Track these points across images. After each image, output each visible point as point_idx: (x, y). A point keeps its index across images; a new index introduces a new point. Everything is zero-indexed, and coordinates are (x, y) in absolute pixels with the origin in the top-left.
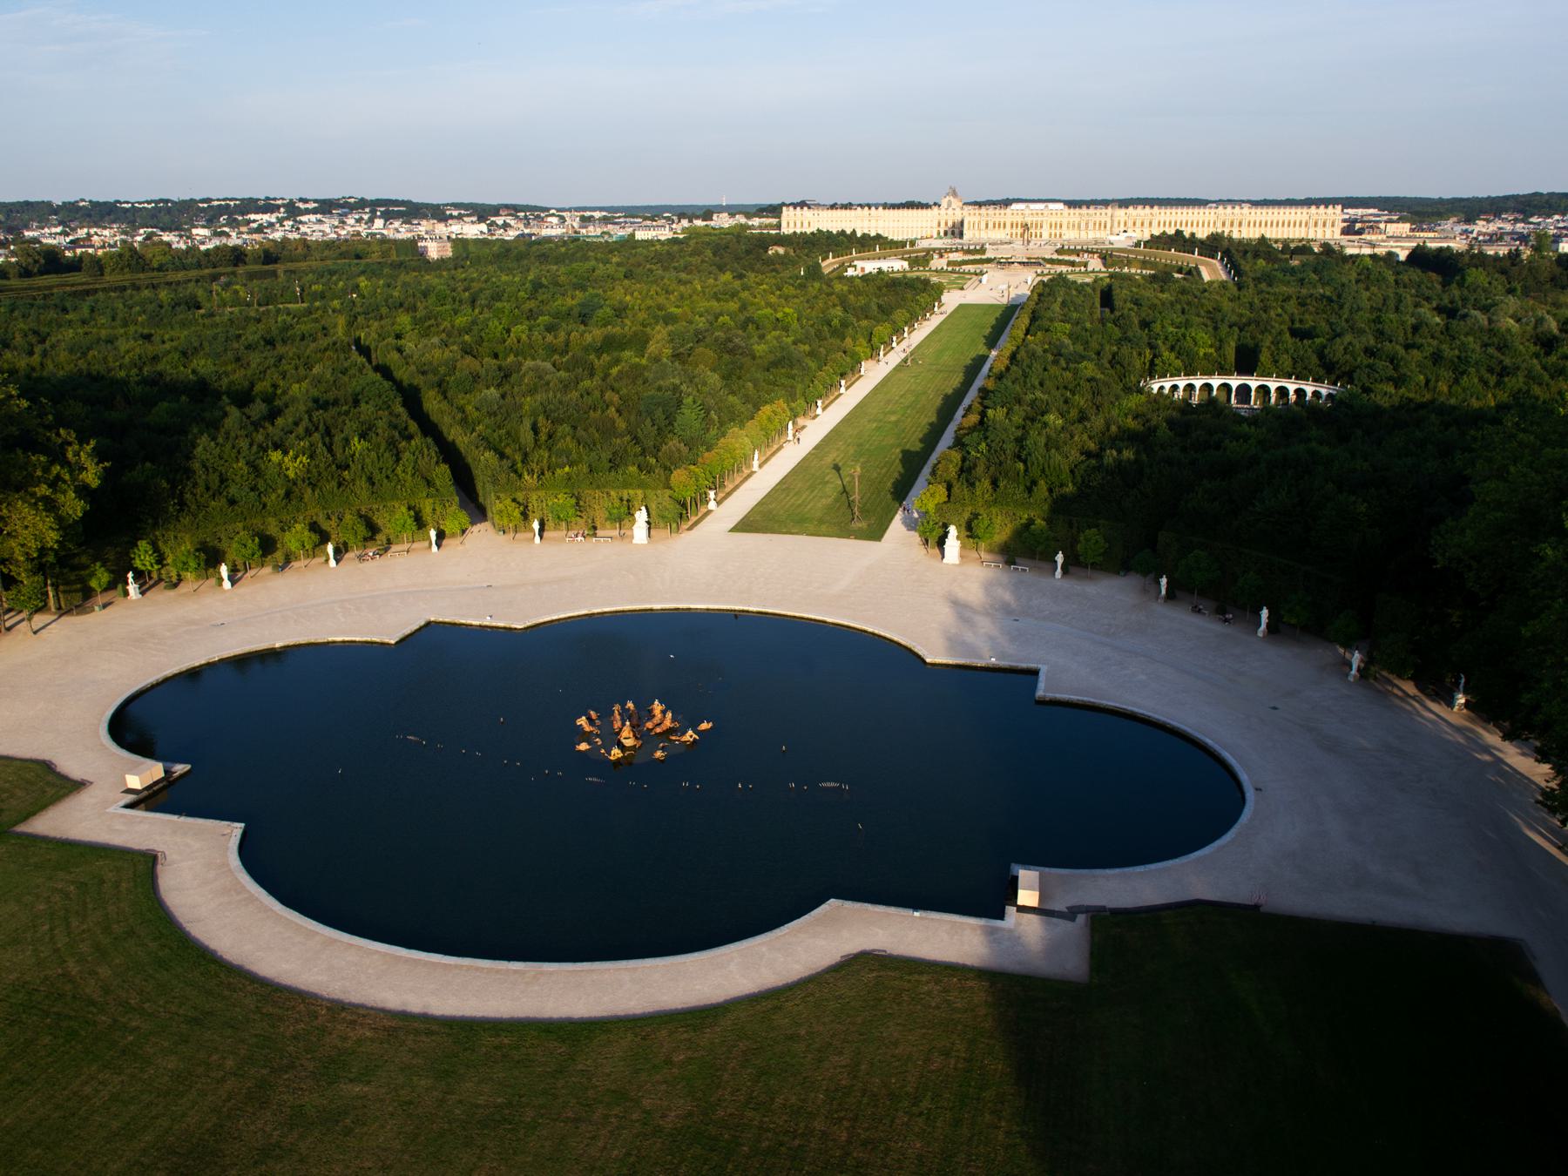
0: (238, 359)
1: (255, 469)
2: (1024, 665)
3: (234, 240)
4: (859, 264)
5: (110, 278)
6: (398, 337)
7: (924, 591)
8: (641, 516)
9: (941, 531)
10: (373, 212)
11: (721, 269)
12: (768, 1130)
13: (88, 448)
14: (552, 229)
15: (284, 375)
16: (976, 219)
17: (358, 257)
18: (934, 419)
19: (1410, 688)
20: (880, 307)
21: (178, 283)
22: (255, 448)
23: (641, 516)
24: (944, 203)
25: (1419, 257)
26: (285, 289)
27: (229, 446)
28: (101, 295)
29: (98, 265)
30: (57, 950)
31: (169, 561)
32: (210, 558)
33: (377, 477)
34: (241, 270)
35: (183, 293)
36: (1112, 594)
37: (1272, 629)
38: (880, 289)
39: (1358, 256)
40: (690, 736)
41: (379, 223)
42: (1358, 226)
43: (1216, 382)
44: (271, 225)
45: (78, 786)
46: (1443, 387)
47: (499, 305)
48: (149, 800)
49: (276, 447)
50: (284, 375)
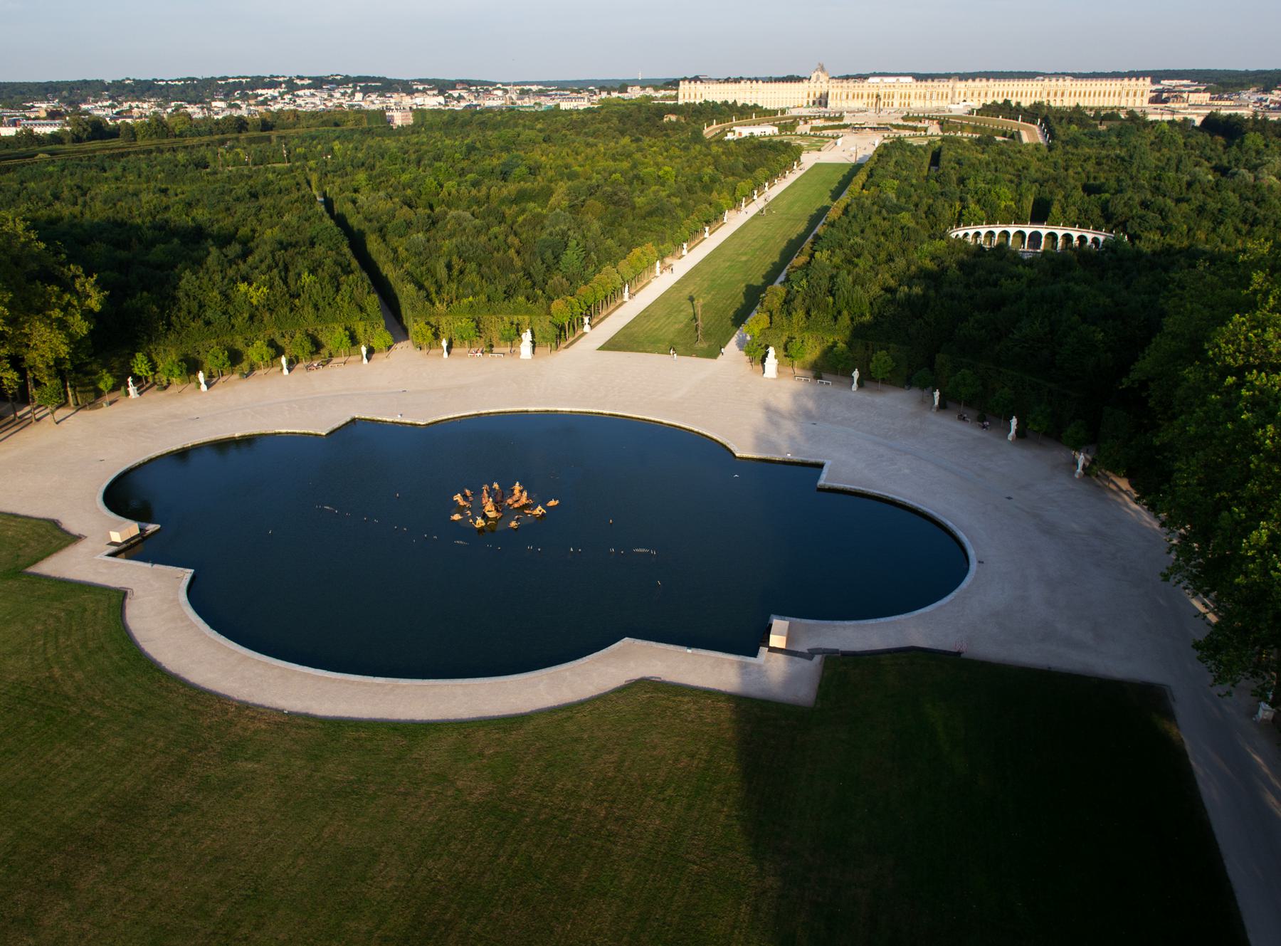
0: (228, 209)
1: (225, 295)
2: (812, 460)
3: (243, 112)
4: (737, 129)
5: (141, 143)
6: (356, 191)
7: (744, 400)
8: (527, 337)
9: (763, 352)
10: (355, 87)
11: (623, 133)
12: (546, 807)
13: (92, 280)
14: (495, 101)
15: (260, 221)
16: (839, 91)
17: (337, 125)
18: (777, 259)
19: (1124, 484)
20: (745, 166)
21: (193, 147)
22: (226, 281)
23: (527, 337)
24: (814, 77)
25: (1212, 124)
26: (275, 151)
27: (206, 278)
28: (132, 157)
29: (132, 132)
30: (46, 659)
31: (160, 369)
32: (191, 366)
33: (321, 304)
34: (243, 136)
35: (197, 155)
36: (895, 404)
37: (1020, 434)
38: (748, 151)
39: (1156, 122)
40: (539, 510)
41: (359, 96)
42: (1165, 95)
43: (1012, 230)
44: (274, 98)
45: (77, 539)
46: (1201, 235)
47: (437, 164)
48: (128, 550)
49: (244, 279)
50: (260, 221)
